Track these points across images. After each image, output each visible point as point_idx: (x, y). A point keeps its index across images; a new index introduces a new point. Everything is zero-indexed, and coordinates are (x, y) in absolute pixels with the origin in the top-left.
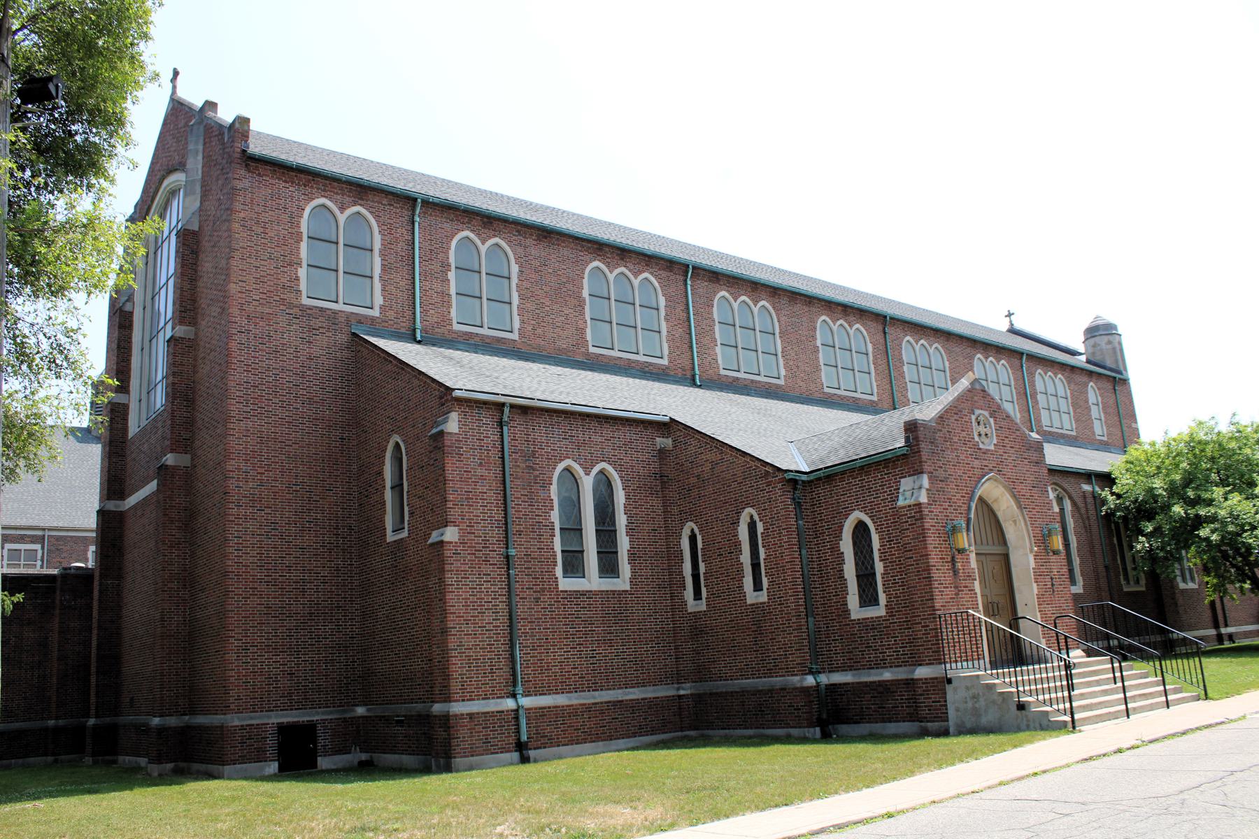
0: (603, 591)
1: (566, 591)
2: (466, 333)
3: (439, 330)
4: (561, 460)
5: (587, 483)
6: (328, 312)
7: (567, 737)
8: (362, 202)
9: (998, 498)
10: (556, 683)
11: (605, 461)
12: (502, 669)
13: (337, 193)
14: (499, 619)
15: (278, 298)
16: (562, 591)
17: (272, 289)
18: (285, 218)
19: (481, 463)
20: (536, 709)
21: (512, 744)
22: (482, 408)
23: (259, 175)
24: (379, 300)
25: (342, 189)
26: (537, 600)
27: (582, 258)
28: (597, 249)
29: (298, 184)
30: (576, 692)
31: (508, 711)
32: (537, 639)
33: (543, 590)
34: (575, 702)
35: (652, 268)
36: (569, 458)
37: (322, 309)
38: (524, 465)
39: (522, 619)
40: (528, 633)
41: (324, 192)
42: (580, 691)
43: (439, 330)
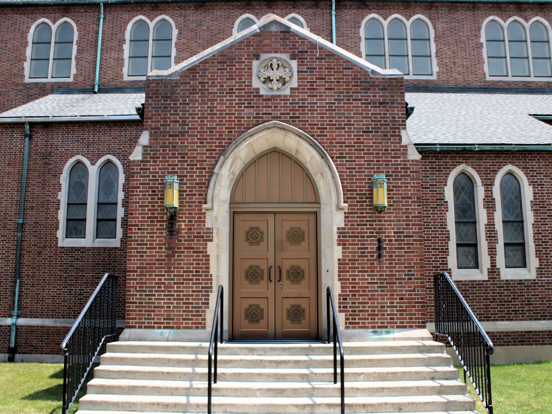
0: (96, 248)
1: (64, 248)
2: (133, 82)
3: (113, 83)
4: (71, 156)
5: (93, 171)
6: (40, 85)
7: (50, 349)
8: (68, 15)
9: (298, 148)
10: (48, 310)
11: (110, 154)
12: (7, 298)
13: (52, 13)
14: (9, 265)
15: (10, 82)
16: (60, 247)
17: (8, 77)
18: (19, 35)
19: (9, 164)
20: (27, 326)
21: (6, 348)
22: (14, 127)
23: (5, 14)
24: (436, 69)
25: (54, 10)
26: (40, 253)
27: (234, 14)
28: (246, 5)
29: (28, 14)
30: (64, 318)
31: (5, 326)
32: (37, 280)
33: (45, 246)
34: (59, 324)
35: (299, 9)
36: (79, 154)
37: (37, 84)
38: (42, 162)
39: (26, 266)
40: (30, 275)
41: (44, 15)
42: (67, 318)
43: (113, 83)
